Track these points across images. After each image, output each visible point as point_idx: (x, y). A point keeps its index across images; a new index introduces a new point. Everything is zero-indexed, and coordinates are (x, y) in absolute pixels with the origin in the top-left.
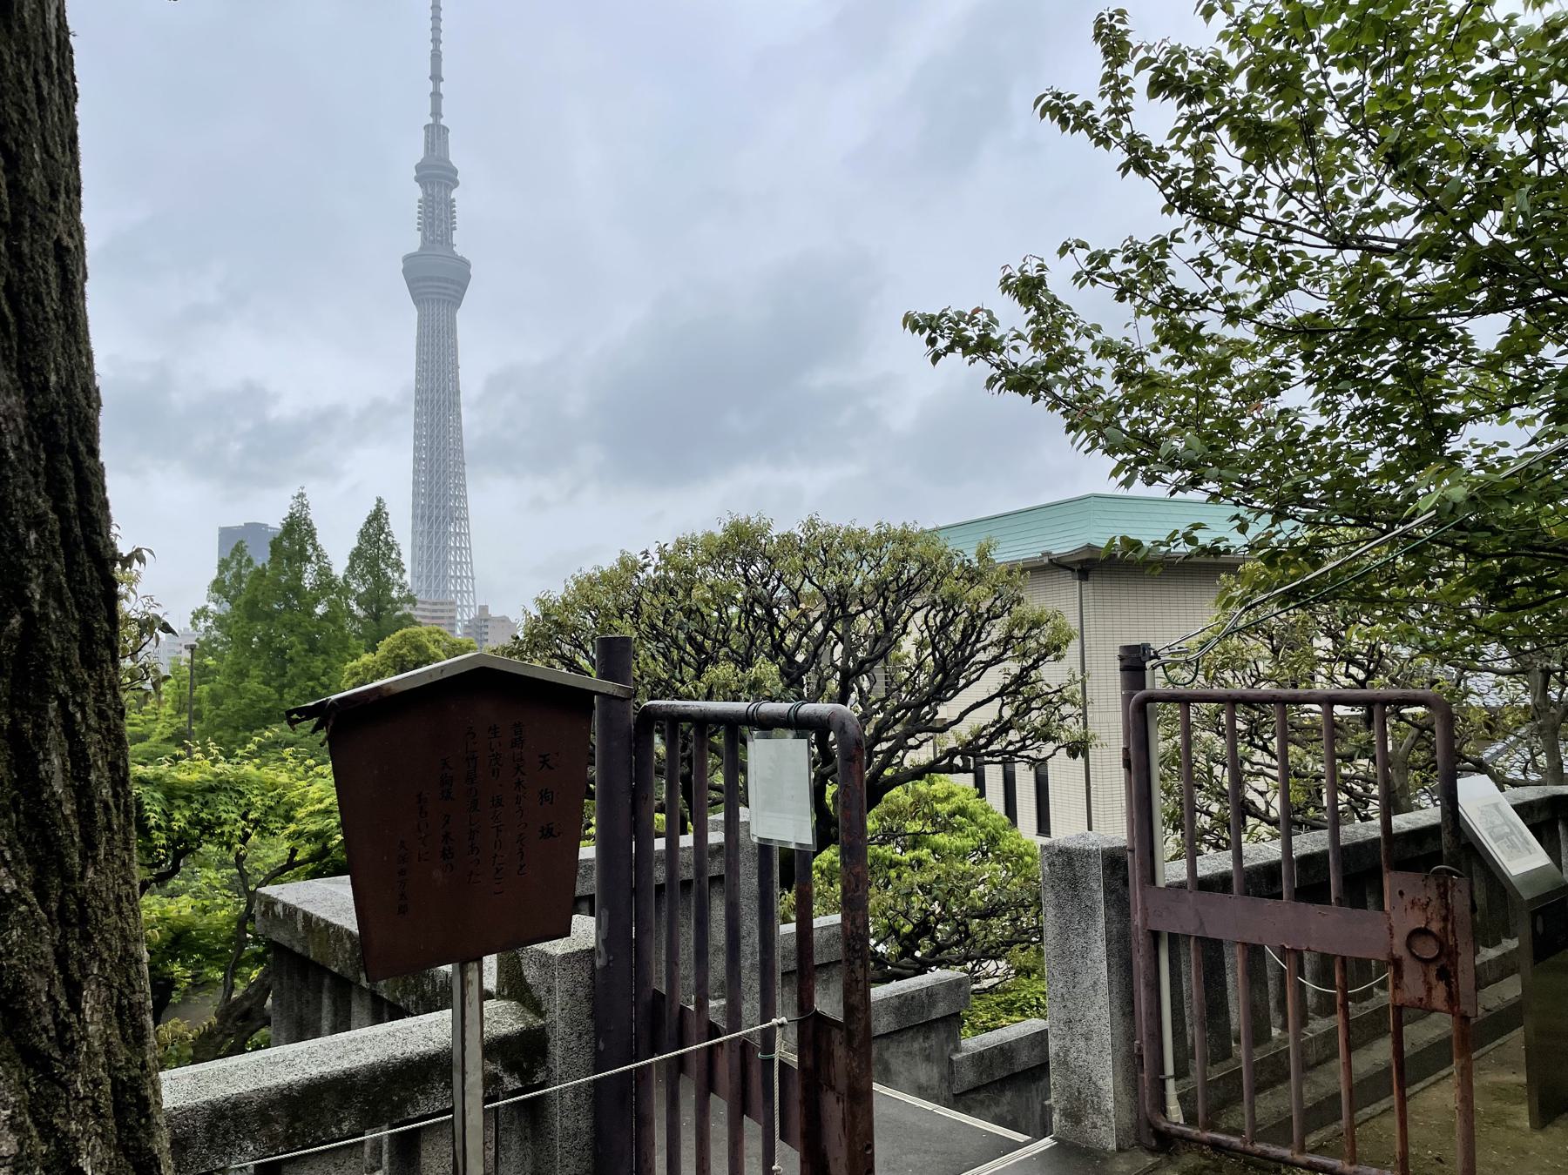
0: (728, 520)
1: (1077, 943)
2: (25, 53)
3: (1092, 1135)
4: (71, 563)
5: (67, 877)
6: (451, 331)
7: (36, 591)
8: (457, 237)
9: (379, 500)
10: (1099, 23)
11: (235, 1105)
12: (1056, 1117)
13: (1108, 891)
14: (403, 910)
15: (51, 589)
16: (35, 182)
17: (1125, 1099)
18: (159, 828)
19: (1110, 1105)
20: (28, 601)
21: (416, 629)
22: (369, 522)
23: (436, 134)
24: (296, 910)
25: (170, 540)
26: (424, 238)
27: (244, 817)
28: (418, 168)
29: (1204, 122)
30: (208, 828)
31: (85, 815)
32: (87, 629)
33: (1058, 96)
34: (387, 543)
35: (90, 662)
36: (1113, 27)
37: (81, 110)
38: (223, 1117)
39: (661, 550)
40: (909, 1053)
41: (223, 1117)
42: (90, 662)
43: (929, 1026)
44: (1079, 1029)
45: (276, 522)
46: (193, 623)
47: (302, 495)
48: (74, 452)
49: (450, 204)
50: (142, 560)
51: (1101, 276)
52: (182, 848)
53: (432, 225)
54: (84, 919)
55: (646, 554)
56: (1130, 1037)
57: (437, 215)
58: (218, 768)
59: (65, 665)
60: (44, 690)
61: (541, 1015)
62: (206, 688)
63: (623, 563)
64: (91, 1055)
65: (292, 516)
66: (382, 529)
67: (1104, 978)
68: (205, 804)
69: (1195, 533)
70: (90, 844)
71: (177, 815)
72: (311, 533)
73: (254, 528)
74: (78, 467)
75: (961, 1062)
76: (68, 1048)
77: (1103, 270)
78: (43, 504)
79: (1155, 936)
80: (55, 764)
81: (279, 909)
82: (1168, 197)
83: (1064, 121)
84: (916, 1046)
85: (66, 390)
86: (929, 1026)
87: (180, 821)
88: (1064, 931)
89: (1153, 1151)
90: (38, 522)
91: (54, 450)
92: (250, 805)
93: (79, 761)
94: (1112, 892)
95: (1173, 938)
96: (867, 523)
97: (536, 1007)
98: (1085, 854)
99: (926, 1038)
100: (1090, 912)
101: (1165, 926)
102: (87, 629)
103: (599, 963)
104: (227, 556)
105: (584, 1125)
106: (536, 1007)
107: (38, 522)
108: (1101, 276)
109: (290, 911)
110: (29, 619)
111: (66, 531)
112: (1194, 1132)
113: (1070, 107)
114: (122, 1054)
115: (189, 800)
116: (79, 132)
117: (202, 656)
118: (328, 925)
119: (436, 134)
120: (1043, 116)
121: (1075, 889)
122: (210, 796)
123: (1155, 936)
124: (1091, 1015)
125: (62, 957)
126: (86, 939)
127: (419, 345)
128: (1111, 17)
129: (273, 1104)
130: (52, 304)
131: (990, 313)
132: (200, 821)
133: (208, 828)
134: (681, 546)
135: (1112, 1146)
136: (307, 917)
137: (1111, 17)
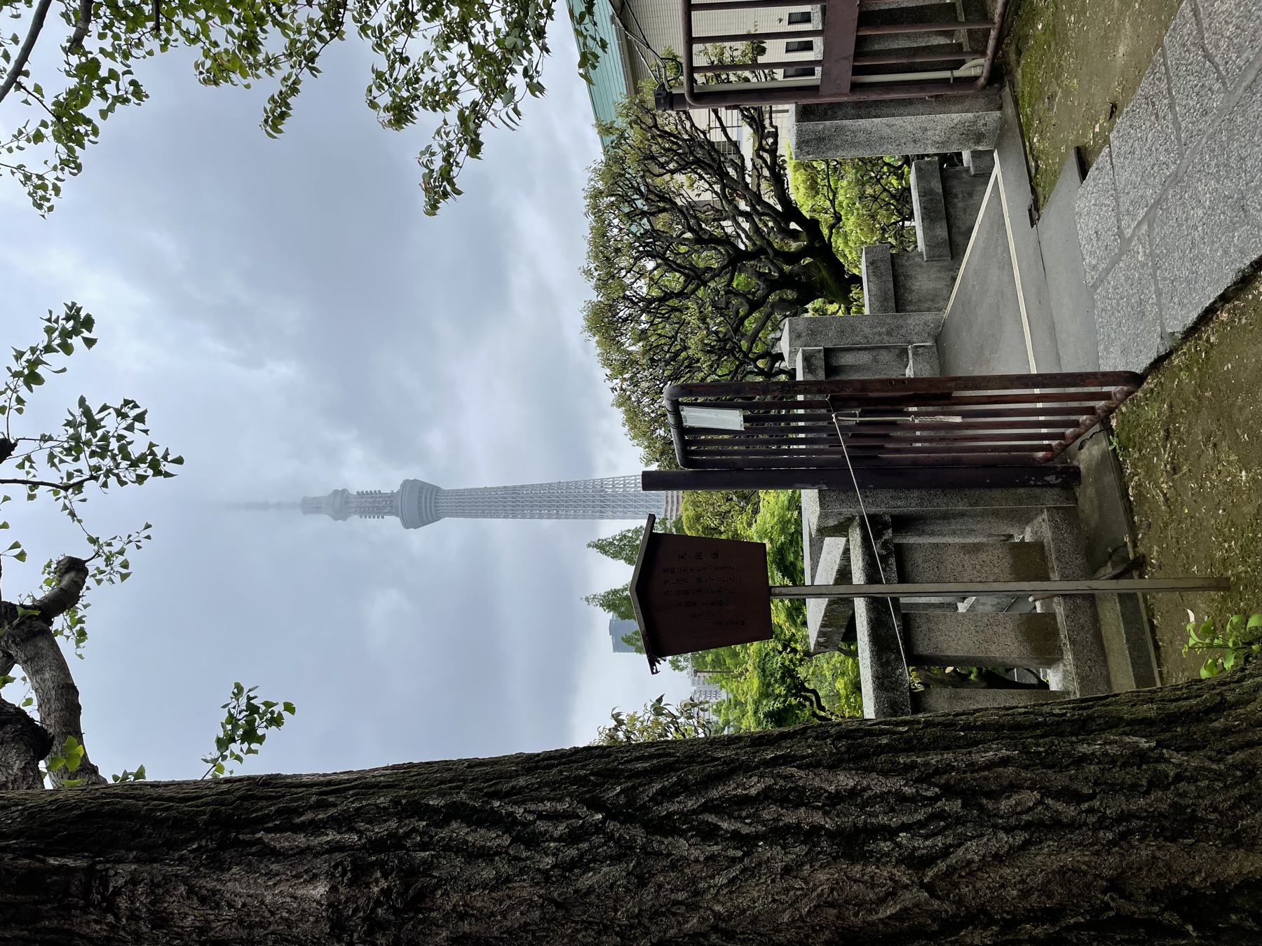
0: (587, 334)
1: (862, 137)
2: (404, 780)
3: (991, 126)
4: (574, 762)
5: (677, 762)
6: (458, 493)
7: (583, 772)
8: (386, 490)
9: (589, 546)
10: (205, 82)
11: (877, 678)
12: (980, 148)
13: (824, 117)
14: (743, 623)
15: (583, 767)
16: (447, 775)
17: (967, 104)
18: (785, 701)
19: (970, 115)
20: (586, 775)
21: (684, 519)
22: (606, 553)
23: (312, 506)
24: (820, 632)
25: (617, 692)
26: (389, 513)
27: (780, 653)
28: (336, 519)
29: (276, 14)
30: (788, 672)
31: (659, 756)
32: (598, 756)
33: (266, 121)
34: (621, 540)
35: (609, 756)
36: (208, 71)
37: (415, 762)
38: (882, 684)
39: (610, 378)
40: (965, 211)
41: (882, 684)
42: (609, 756)
43: (947, 193)
44: (919, 135)
45: (610, 616)
46: (682, 670)
47: (587, 599)
48: (538, 761)
49: (361, 495)
50: (619, 714)
51: (391, 76)
52: (798, 688)
53: (378, 508)
54: (692, 756)
55: (613, 389)
56: (922, 100)
57: (374, 504)
58: (750, 669)
59: (608, 763)
60: (615, 769)
61: (854, 517)
62: (728, 661)
63: (620, 406)
64: (737, 754)
65: (601, 605)
66: (611, 544)
67: (885, 120)
68: (772, 675)
69: (577, 14)
70: (669, 755)
71: (777, 692)
72: (615, 592)
73: (613, 630)
74: (543, 760)
75: (976, 168)
76: (732, 761)
77: (387, 76)
78: (555, 771)
79: (855, 87)
80: (640, 766)
81: (821, 640)
82: (332, 37)
83: (283, 116)
84: (960, 205)
85: (517, 764)
86: (947, 193)
87: (780, 690)
88: (853, 145)
89: (1002, 87)
90: (561, 772)
91: (537, 768)
92: (774, 649)
93: (638, 759)
94: (826, 113)
95: (857, 71)
96: (586, 225)
97: (850, 520)
98: (800, 133)
99: (956, 196)
100: (839, 130)
101: (849, 77)
102: (598, 756)
103: (825, 488)
104: (633, 648)
105: (916, 493)
106: (850, 520)
107: (561, 772)
108: (391, 76)
109: (821, 634)
110: (592, 774)
111: (564, 764)
112: (989, 52)
113: (273, 112)
114: (742, 744)
115: (769, 685)
116: (81, 700)
117: (705, 664)
118: (825, 615)
119: (312, 506)
120: (280, 131)
121: (824, 139)
122: (768, 673)
123: (855, 87)
124: (909, 128)
125: (703, 763)
126: (699, 756)
127: (471, 517)
128: (201, 73)
129: (879, 659)
130: (488, 769)
131: (423, 153)
132: (783, 677)
133: (788, 672)
134: (607, 362)
135: (998, 113)
136: (822, 626)
137: (201, 73)
